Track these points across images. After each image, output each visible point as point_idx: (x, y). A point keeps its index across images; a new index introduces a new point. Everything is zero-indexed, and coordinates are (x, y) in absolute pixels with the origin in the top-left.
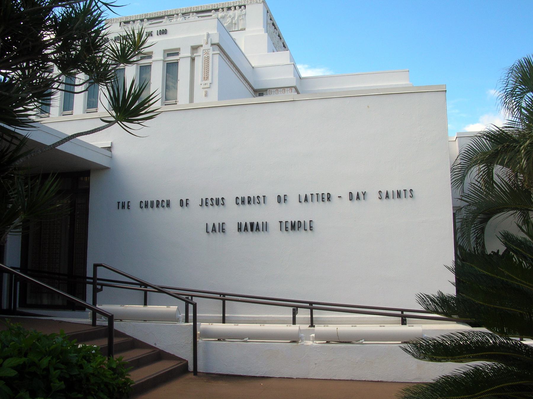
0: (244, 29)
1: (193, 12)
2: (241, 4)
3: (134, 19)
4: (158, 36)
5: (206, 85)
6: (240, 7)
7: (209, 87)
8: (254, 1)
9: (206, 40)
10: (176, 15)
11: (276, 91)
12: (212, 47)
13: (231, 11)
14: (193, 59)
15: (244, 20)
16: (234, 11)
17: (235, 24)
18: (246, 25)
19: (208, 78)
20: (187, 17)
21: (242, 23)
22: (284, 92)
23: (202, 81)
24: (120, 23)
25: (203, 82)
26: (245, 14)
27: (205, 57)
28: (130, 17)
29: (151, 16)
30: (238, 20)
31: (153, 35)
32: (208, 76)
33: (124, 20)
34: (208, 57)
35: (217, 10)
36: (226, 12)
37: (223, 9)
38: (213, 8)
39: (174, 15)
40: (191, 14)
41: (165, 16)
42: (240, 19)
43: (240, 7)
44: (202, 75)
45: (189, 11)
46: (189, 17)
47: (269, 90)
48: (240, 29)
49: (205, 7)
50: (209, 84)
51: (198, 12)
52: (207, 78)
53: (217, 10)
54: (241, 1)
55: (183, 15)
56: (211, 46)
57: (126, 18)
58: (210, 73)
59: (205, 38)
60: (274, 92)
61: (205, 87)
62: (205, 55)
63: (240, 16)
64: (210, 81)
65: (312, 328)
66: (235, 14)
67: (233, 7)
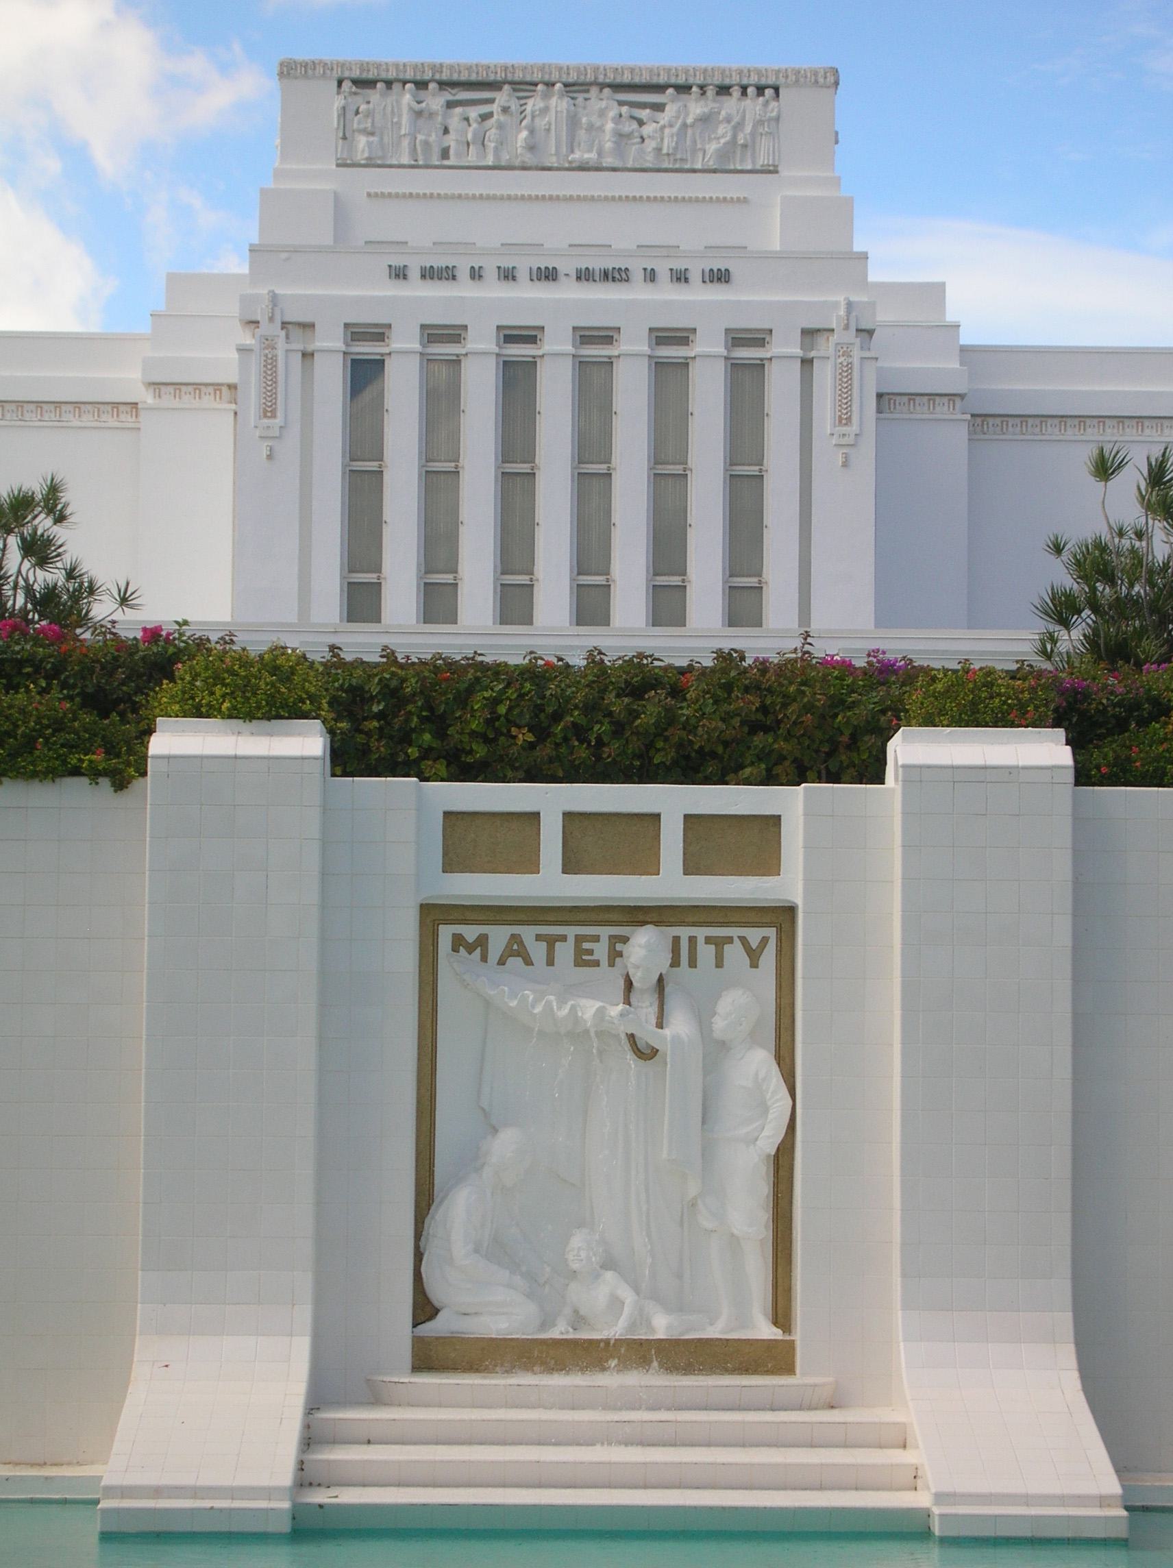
0: (773, 170)
1: (603, 86)
2: (763, 81)
3: (392, 75)
4: (703, 285)
5: (846, 438)
6: (760, 90)
7: (852, 443)
8: (808, 80)
9: (846, 318)
10: (545, 87)
11: (909, 402)
12: (858, 340)
13: (729, 97)
14: (807, 363)
15: (774, 138)
16: (739, 99)
17: (745, 146)
18: (779, 153)
19: (849, 419)
20: (581, 97)
21: (769, 149)
22: (931, 408)
23: (835, 427)
24: (340, 83)
25: (837, 428)
26: (777, 119)
27: (841, 363)
28: (378, 66)
29: (455, 77)
30: (753, 134)
31: (690, 280)
32: (850, 416)
33: (356, 74)
34: (851, 363)
35: (683, 89)
36: (714, 101)
37: (702, 87)
38: (673, 81)
39: (536, 85)
40: (594, 91)
41: (505, 83)
42: (761, 130)
43: (760, 90)
44: (835, 412)
45: (590, 77)
46: (586, 99)
47: (890, 400)
48: (758, 167)
49: (644, 72)
50: (852, 436)
51: (617, 87)
52: (846, 419)
53: (683, 89)
54: (764, 72)
55: (568, 89)
56: (857, 337)
57: (364, 66)
58: (855, 407)
59: (842, 312)
60: (904, 404)
61: (844, 443)
62: (842, 359)
63: (760, 122)
64: (854, 428)
65: (660, 1030)
66: (744, 111)
67: (736, 88)
